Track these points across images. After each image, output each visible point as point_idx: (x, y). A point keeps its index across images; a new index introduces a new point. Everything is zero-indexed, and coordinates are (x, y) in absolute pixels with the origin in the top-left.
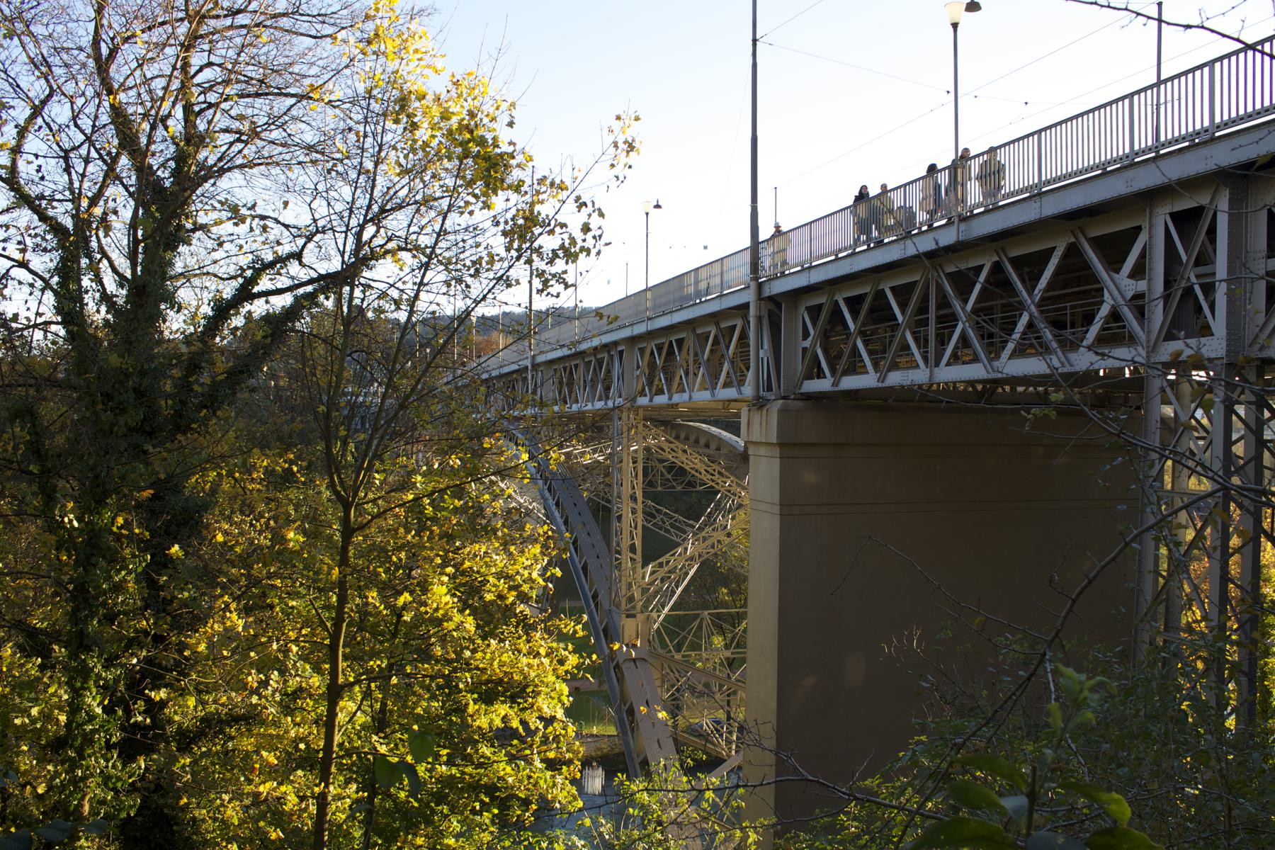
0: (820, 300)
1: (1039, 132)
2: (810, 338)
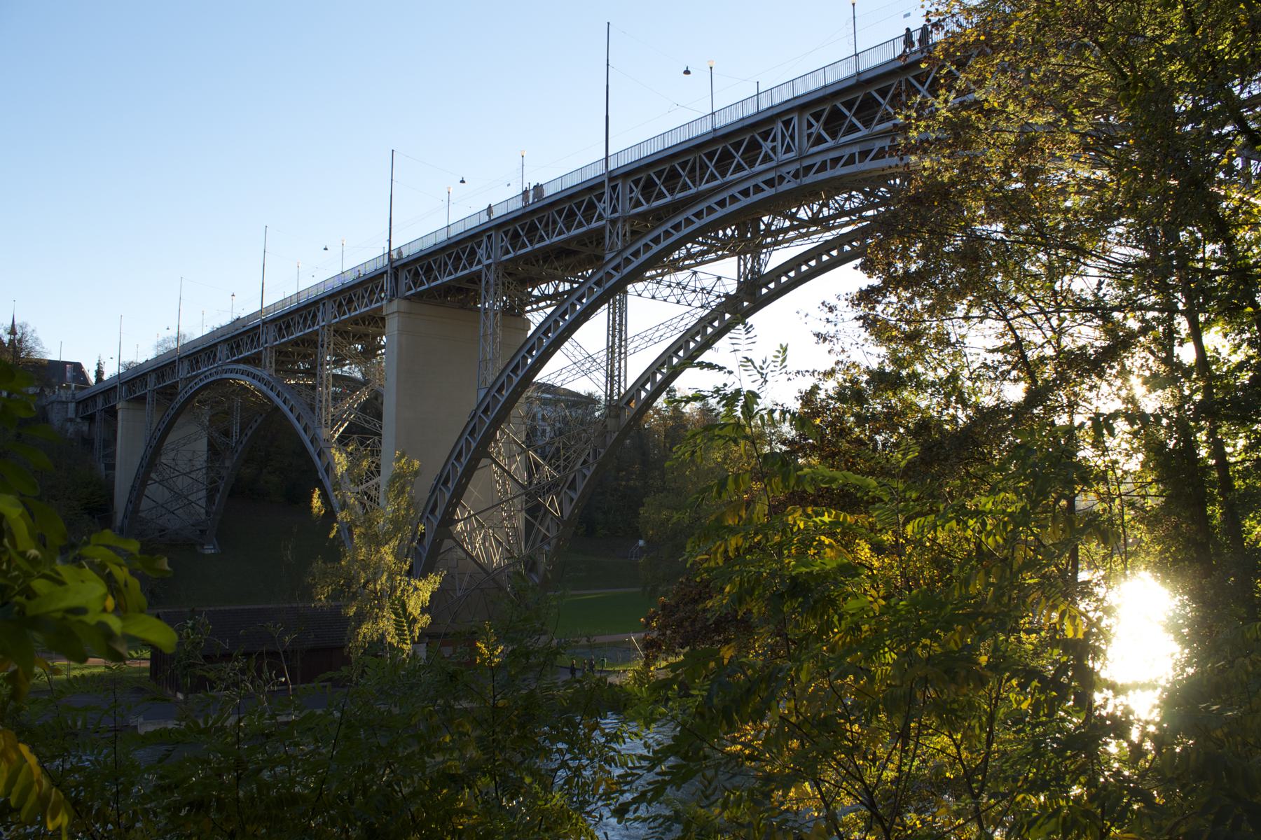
0: (667, 166)
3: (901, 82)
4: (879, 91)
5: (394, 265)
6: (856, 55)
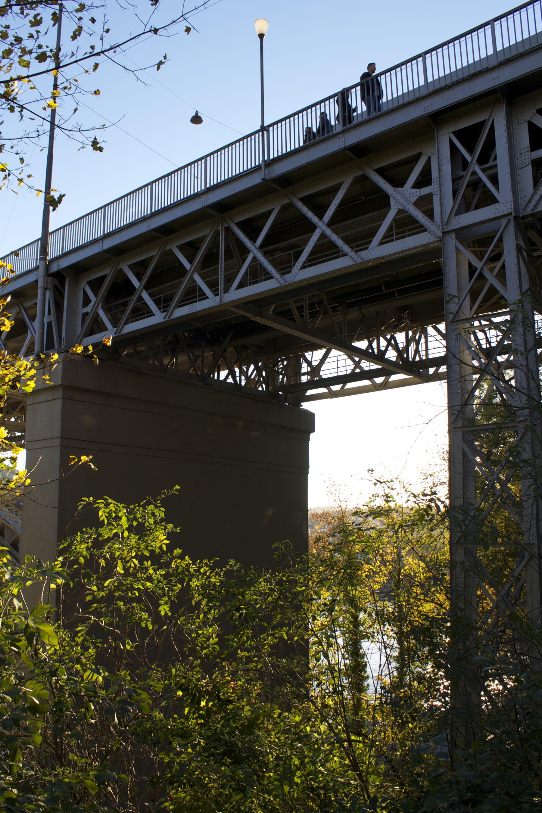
0: (108, 271)
1: (205, 157)
2: (92, 304)
3: (217, 235)
4: (245, 226)
5: (55, 268)
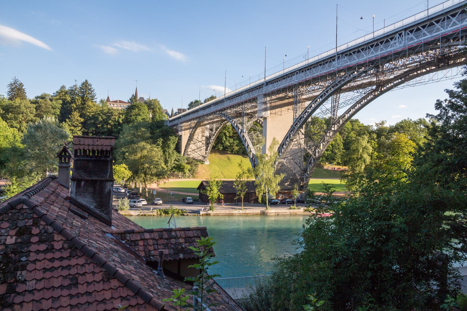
3: (445, 18)
6: (428, 9)
